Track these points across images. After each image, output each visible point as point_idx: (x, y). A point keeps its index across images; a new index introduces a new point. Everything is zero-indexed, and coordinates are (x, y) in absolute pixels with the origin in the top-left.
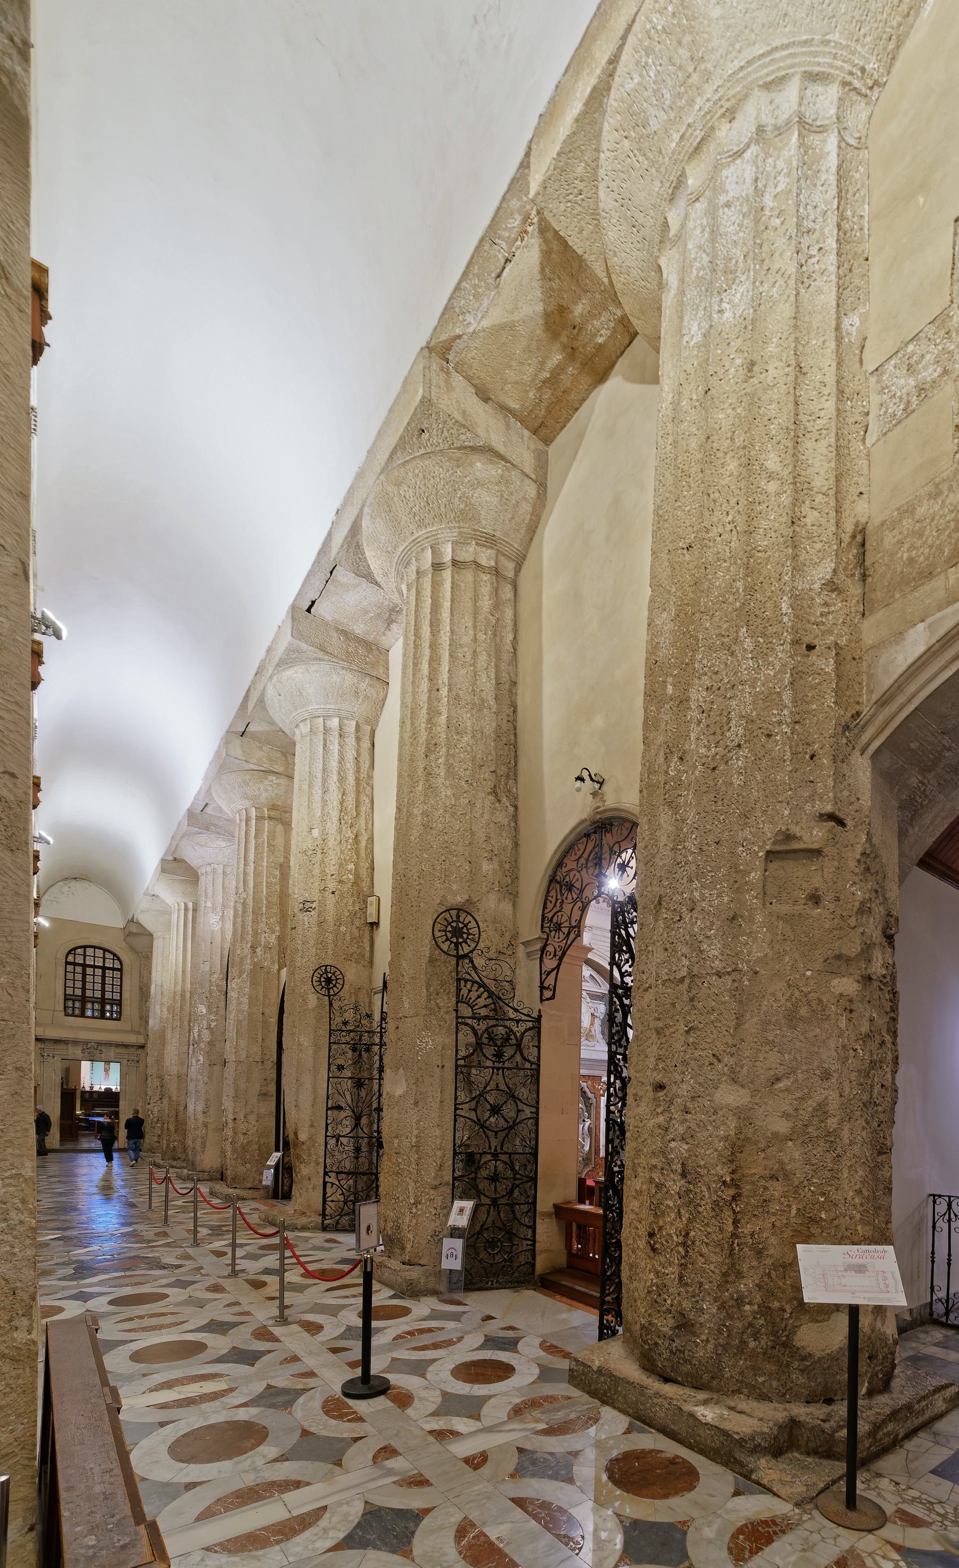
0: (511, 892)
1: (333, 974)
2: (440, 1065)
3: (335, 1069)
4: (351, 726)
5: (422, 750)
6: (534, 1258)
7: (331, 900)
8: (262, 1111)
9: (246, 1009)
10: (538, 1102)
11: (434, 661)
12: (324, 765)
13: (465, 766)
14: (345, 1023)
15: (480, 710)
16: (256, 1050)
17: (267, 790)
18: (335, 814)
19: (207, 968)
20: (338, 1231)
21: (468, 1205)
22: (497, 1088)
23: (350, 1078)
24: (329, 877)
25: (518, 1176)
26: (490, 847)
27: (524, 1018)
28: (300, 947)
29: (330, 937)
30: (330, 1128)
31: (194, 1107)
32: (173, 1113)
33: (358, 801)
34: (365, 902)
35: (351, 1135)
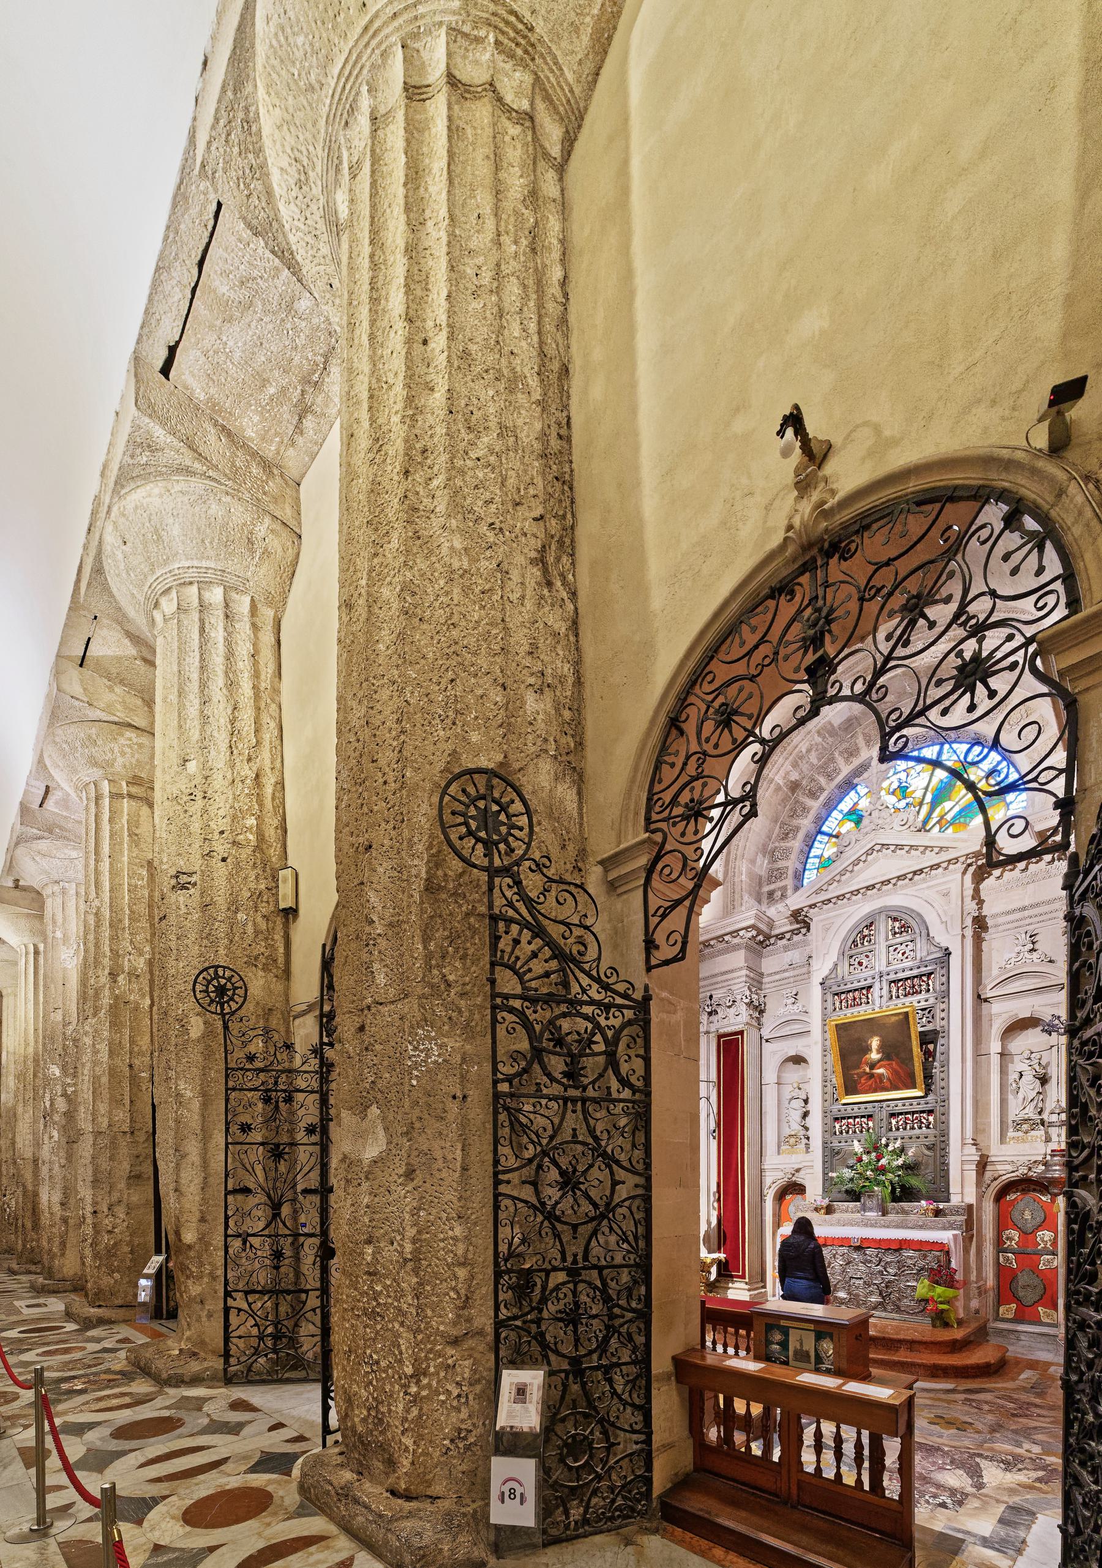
0: (573, 766)
1: (229, 979)
2: (459, 1094)
3: (237, 1129)
4: (243, 604)
5: (393, 469)
6: (649, 1467)
7: (221, 871)
8: (135, 1199)
9: (105, 1059)
10: (648, 1166)
11: (416, 283)
12: (202, 660)
13: (487, 496)
14: (251, 1058)
15: (511, 391)
16: (122, 1115)
17: (122, 752)
18: (222, 739)
19: (59, 1018)
20: (250, 1382)
21: (534, 1378)
22: (575, 1140)
23: (262, 1144)
24: (216, 836)
25: (616, 1311)
26: (538, 667)
27: (619, 1001)
28: (173, 945)
29: (221, 930)
30: (231, 1223)
31: (49, 1197)
32: (30, 1206)
33: (257, 721)
34: (275, 878)
35: (266, 1232)
